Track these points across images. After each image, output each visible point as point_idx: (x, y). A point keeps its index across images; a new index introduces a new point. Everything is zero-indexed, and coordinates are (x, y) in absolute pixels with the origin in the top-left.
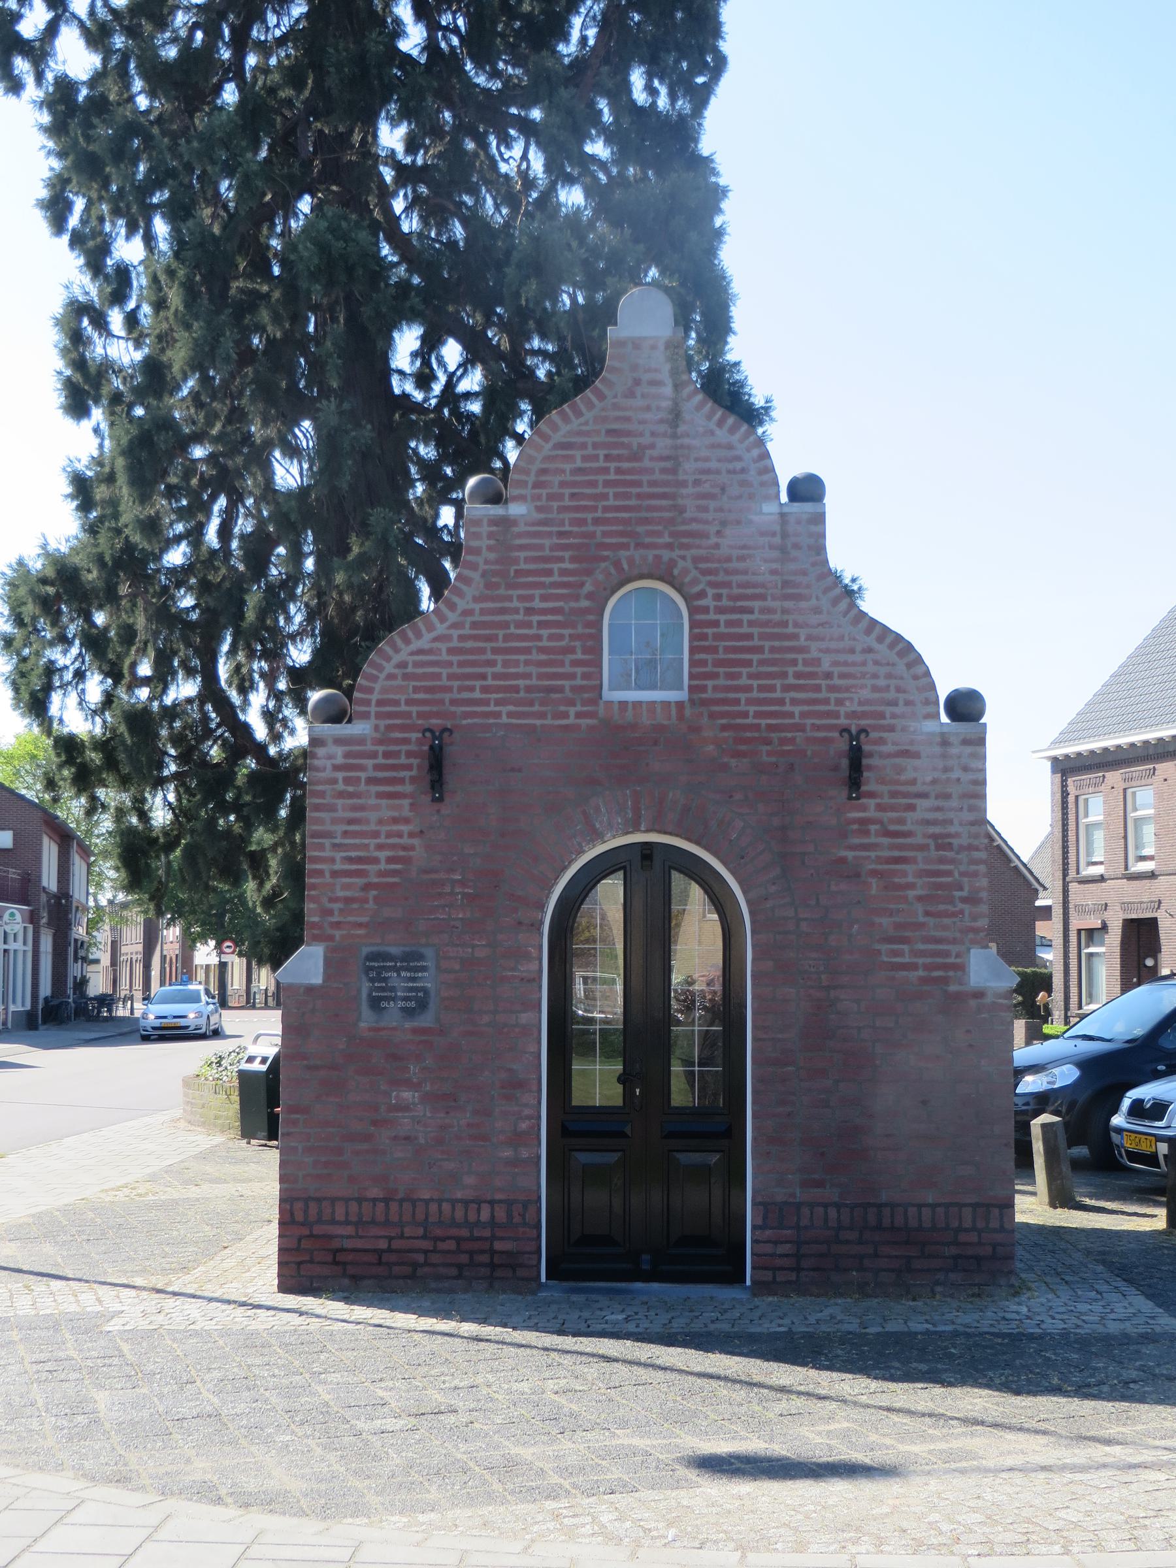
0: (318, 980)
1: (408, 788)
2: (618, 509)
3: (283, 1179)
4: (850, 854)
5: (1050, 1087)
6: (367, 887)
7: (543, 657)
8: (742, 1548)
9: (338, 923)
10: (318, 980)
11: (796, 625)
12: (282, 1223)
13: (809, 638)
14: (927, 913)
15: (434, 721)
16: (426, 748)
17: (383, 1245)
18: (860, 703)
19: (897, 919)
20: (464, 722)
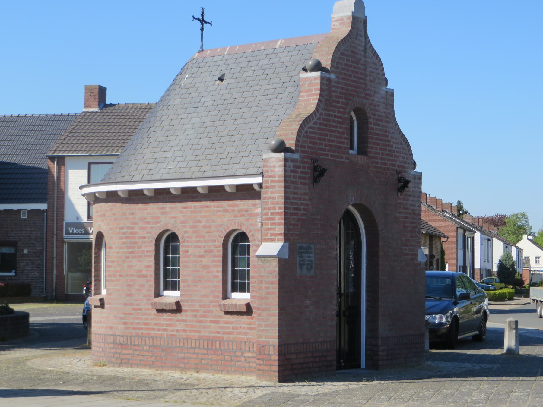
0: (287, 257)
1: (307, 181)
2: (354, 82)
3: (280, 337)
4: (397, 215)
5: (264, 290)
6: (298, 220)
7: (338, 135)
8: (116, 352)
9: (292, 234)
10: (287, 257)
11: (389, 133)
12: (279, 355)
13: (391, 138)
14: (411, 236)
15: (314, 156)
16: (312, 166)
17: (302, 361)
18: (400, 162)
19: (212, 254)
20: (321, 157)
